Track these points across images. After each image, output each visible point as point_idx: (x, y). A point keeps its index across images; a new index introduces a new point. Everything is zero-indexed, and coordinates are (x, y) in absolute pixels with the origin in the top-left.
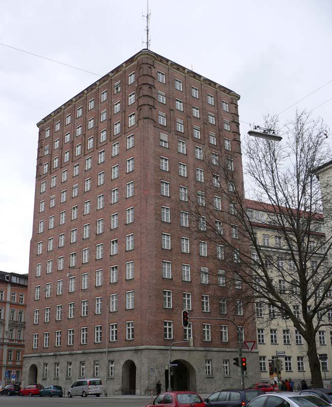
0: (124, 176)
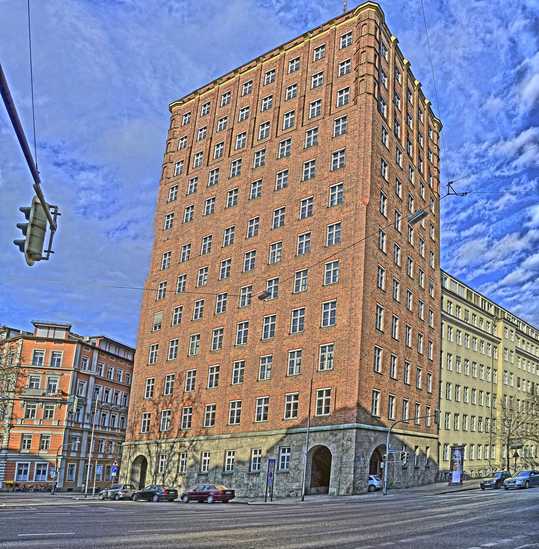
0: (326, 175)
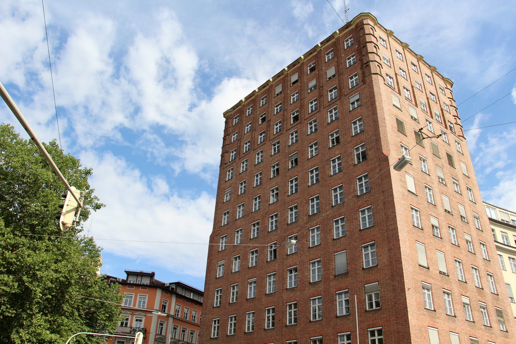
0: (349, 140)
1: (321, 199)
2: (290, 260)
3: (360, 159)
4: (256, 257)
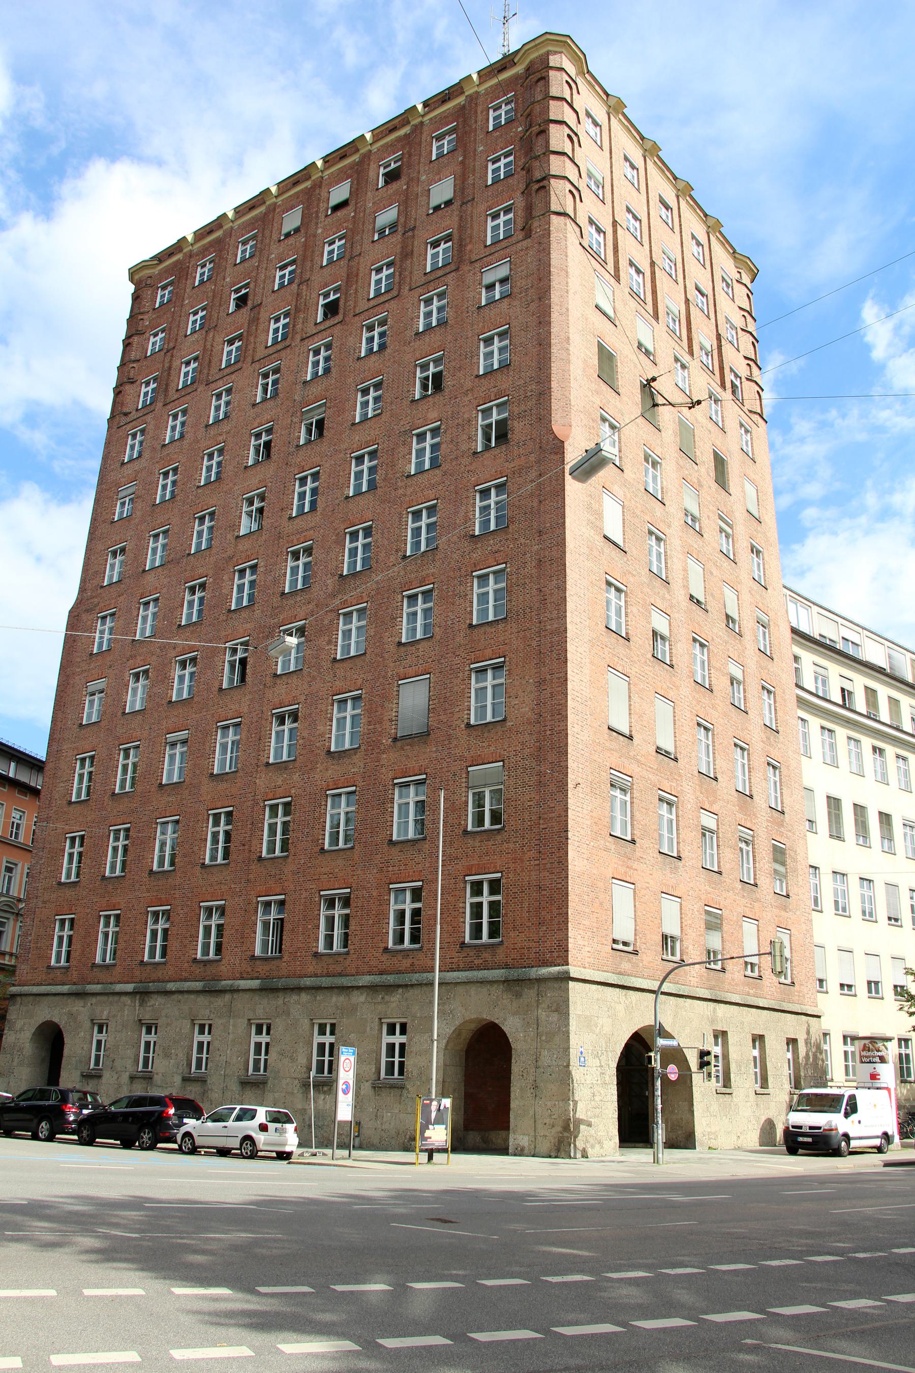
0: (468, 384)
1: (376, 535)
2: (281, 690)
3: (489, 440)
4: (192, 674)
